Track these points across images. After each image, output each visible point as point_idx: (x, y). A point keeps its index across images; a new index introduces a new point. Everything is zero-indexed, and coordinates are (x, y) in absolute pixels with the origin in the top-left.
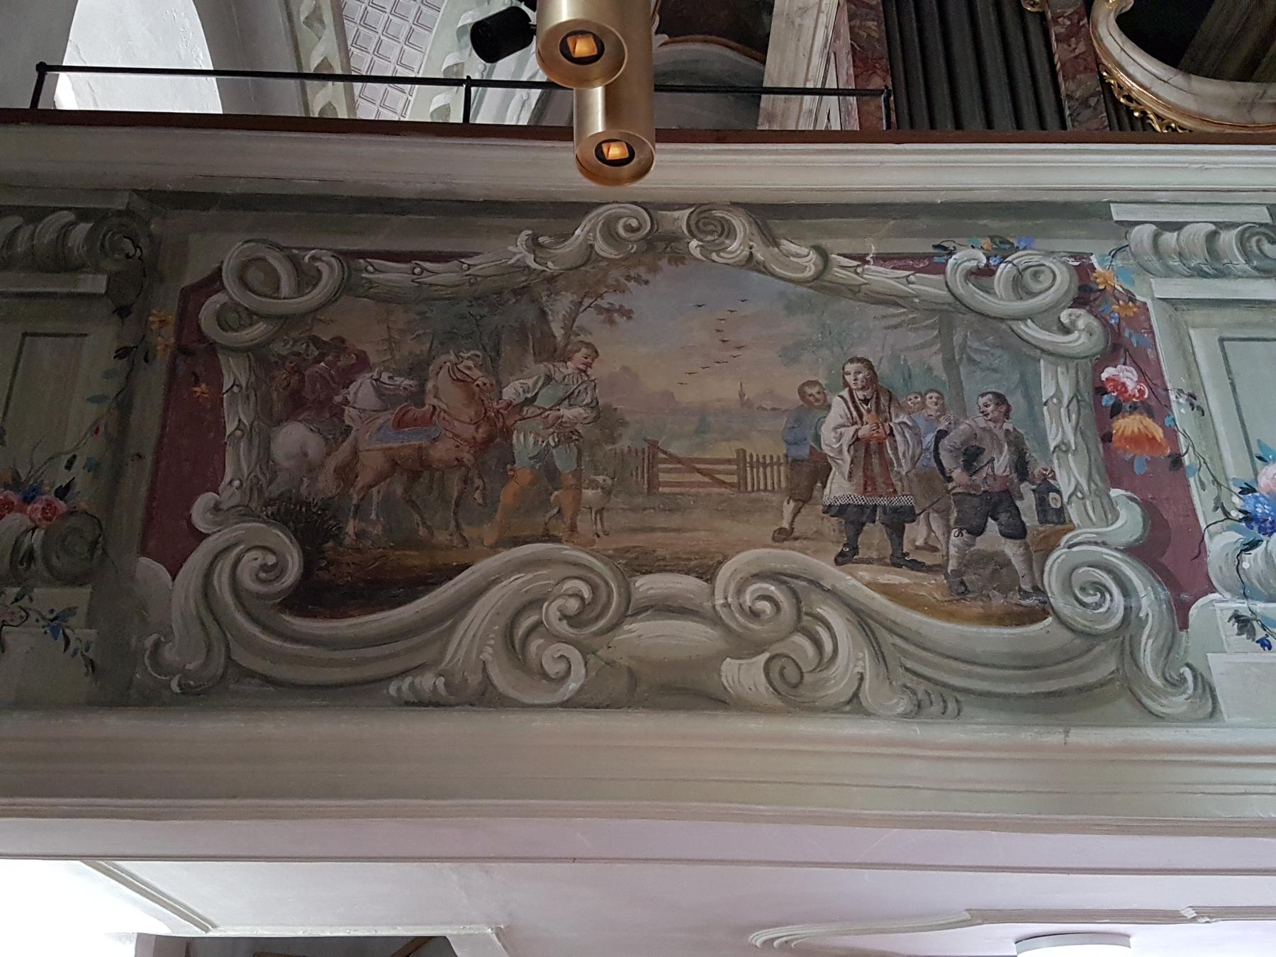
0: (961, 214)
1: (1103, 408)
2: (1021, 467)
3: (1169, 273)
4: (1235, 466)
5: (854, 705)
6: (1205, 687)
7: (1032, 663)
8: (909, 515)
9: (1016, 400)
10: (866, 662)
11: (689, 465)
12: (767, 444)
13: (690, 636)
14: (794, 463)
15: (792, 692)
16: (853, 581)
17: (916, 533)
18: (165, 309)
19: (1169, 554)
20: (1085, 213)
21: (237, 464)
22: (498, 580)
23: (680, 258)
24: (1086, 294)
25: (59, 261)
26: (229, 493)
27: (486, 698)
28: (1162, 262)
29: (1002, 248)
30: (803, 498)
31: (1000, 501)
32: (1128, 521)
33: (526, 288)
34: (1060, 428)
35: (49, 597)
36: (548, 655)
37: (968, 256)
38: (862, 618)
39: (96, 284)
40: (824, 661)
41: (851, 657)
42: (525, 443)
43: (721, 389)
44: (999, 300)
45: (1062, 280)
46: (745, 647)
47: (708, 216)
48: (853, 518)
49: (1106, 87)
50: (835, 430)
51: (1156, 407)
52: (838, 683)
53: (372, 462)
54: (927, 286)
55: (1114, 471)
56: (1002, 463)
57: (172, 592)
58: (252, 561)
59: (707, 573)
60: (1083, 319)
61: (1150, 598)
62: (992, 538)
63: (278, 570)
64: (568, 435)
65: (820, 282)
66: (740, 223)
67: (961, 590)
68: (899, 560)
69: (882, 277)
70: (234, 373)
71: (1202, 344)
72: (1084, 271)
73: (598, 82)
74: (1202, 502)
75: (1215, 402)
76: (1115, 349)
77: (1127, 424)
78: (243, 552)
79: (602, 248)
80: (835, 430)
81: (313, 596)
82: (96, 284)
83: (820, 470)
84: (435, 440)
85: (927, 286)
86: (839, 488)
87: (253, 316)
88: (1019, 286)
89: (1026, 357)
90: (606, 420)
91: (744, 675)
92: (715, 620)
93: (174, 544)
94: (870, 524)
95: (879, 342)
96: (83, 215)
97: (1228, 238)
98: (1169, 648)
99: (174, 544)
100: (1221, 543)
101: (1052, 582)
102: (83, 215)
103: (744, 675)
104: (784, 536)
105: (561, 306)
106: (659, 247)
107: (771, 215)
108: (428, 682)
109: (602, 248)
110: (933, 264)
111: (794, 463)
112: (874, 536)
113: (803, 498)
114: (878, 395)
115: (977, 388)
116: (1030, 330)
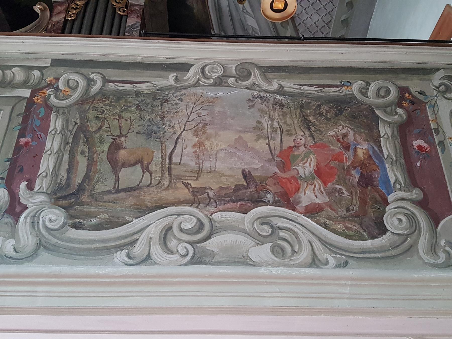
50: (371, 153)
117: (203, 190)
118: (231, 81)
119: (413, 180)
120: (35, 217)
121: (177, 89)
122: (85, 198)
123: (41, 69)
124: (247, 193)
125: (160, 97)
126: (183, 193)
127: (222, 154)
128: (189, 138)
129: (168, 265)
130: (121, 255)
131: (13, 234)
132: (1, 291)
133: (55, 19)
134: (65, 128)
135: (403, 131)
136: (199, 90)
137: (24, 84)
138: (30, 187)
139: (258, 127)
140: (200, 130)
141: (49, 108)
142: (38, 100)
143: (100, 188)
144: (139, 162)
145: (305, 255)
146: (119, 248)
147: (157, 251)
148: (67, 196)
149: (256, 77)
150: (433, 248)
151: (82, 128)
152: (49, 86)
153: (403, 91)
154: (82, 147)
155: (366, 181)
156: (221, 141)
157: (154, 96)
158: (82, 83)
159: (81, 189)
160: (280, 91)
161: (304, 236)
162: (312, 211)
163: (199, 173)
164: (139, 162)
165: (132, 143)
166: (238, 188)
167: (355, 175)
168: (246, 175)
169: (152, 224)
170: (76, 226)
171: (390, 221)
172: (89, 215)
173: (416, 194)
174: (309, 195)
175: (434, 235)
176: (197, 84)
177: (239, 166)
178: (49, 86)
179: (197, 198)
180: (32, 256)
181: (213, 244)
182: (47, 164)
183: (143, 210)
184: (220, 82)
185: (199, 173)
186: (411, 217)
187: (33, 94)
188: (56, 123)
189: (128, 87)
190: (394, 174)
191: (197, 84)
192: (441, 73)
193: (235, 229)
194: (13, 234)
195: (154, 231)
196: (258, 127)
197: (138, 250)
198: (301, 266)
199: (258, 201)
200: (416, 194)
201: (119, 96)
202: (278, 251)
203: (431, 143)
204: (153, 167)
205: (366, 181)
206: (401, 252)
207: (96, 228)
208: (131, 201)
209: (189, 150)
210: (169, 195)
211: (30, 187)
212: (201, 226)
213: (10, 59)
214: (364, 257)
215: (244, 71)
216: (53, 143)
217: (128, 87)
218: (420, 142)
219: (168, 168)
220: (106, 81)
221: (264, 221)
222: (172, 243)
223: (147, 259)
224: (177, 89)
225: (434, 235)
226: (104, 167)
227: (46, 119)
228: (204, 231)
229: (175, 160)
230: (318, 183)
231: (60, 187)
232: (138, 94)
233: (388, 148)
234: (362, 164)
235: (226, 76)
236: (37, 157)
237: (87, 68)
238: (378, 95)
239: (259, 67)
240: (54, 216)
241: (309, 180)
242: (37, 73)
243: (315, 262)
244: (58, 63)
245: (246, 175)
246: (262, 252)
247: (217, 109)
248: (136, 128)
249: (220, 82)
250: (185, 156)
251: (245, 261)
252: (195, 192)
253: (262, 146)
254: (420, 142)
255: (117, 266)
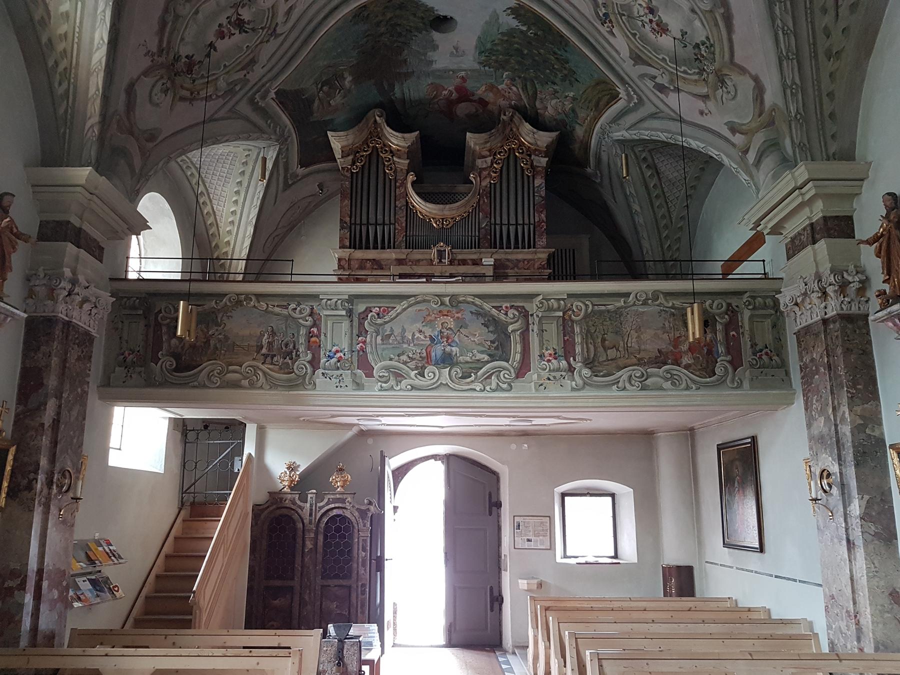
0: (293, 297)
1: (310, 335)
2: (294, 347)
3: (328, 309)
4: (329, 348)
5: (261, 387)
6: (315, 384)
7: (290, 380)
8: (275, 355)
9: (296, 335)
10: (264, 381)
11: (239, 346)
12: (253, 343)
13: (237, 376)
14: (257, 346)
15: (252, 386)
16: (263, 367)
17: (275, 359)
18: (152, 318)
19: (314, 363)
20: (315, 297)
21: (165, 346)
22: (207, 366)
23: (242, 305)
24: (311, 314)
25: (133, 308)
26: (164, 353)
27: (204, 386)
28: (327, 307)
29: (299, 304)
30: (258, 352)
31: (290, 354)
32: (309, 357)
33: (213, 312)
34: (302, 340)
35: (138, 369)
36: (214, 379)
37: (293, 306)
38: (264, 373)
39: (140, 312)
40: (258, 380)
41: (262, 379)
42: (212, 342)
43: (247, 332)
44: (297, 315)
45: (308, 311)
46: (245, 378)
47: (248, 297)
48: (266, 356)
49: (407, 203)
50: (265, 341)
51: (318, 336)
52: (260, 385)
53: (187, 345)
54: (285, 312)
55: (309, 348)
56: (291, 347)
57: (156, 368)
58: (169, 363)
59: (241, 366)
60: (310, 319)
61: (309, 370)
62: (288, 360)
63: (171, 365)
64: (220, 341)
65: (266, 311)
66: (253, 298)
67: (281, 369)
68: (272, 364)
69: (277, 310)
70: (164, 329)
71: (329, 324)
72: (312, 309)
73: (251, 131)
74: (322, 353)
75: (328, 336)
76: (315, 325)
77: (313, 339)
78: (167, 362)
79: (228, 304)
80: (265, 341)
81: (177, 370)
82: (140, 312)
83: (262, 347)
84: (447, 360)
85: (285, 312)
86: (264, 351)
87: (167, 318)
88: (301, 312)
89: (299, 326)
90: (226, 338)
91: (245, 383)
92: (241, 374)
93: (156, 360)
94: (268, 358)
95: (275, 323)
96: (137, 298)
97: (339, 302)
98: (310, 378)
99: (156, 360)
100: (323, 360)
101: (295, 367)
102: (137, 298)
103: (245, 383)
104: (254, 359)
105: (220, 315)
106: (239, 303)
107: (260, 296)
108: (196, 383)
109: (228, 304)
110: (528, 177)
111: (257, 346)
112: (269, 359)
113: (258, 352)
114: (273, 333)
115: (290, 332)
116: (301, 321)
117: (642, 359)
118: (650, 301)
119: (728, 352)
120: (580, 372)
121: (626, 308)
122: (596, 364)
123: (563, 299)
124: (660, 360)
125: (618, 312)
126: (635, 361)
127: (649, 342)
128: (634, 334)
129: (632, 391)
130: (615, 387)
131: (574, 380)
132: (299, 672)
133: (484, 184)
134: (581, 331)
135: (727, 327)
136: (635, 308)
137: (558, 309)
138: (575, 360)
139: (664, 327)
140: (638, 330)
141: (573, 321)
142: (567, 317)
143: (601, 359)
144: (614, 346)
145: (684, 385)
146: (614, 384)
147: (627, 385)
148: (589, 363)
149: (662, 300)
150: (733, 381)
151: (588, 331)
152: (569, 309)
153: (729, 305)
154: (590, 341)
155: (710, 352)
156: (647, 335)
157: (615, 312)
158: (583, 307)
159: (594, 360)
160: (673, 307)
161: (684, 377)
162: (687, 367)
163: (639, 351)
164: (614, 346)
165: (609, 337)
166: (656, 357)
167: (705, 349)
168: (659, 351)
169: (624, 374)
170: (596, 376)
171: (717, 371)
172: (600, 371)
173: (729, 358)
174: (686, 360)
175: (734, 376)
176: (634, 305)
177: (657, 347)
178: (569, 309)
179: (640, 363)
180: (583, 388)
181: (649, 382)
182: (578, 349)
183: (620, 368)
184: (645, 303)
185: (639, 351)
186: (726, 368)
187: (564, 314)
188: (577, 329)
189: (603, 308)
190: (721, 349)
191: (634, 305)
192: (747, 294)
193: (657, 375)
194: (574, 380)
195: (625, 377)
196: (664, 327)
197: (620, 385)
198: (682, 390)
199: (665, 364)
200: (729, 358)
201: (601, 313)
202: (673, 384)
203: (738, 333)
204: (620, 349)
205: (710, 352)
206: (721, 383)
207: (603, 376)
208: (614, 365)
209: (634, 340)
210: (629, 361)
211: (575, 360)
212: (643, 375)
213: (549, 295)
214: (706, 386)
215: (656, 295)
216: (578, 339)
217: (603, 308)
218: (734, 333)
219: (627, 349)
220: (593, 305)
221: (668, 372)
222: (633, 382)
223: (624, 389)
224: (626, 308)
225: (734, 376)
226: (601, 349)
227: (572, 327)
228: (645, 377)
229: (629, 345)
230: (690, 354)
231: (586, 360)
232: (608, 311)
233: (720, 336)
234: (708, 345)
235: (647, 299)
236: (574, 345)
237: (895, 527)
238: (717, 308)
239: (663, 293)
240: (586, 372)
241: (686, 353)
242: (562, 302)
243: (688, 388)
244: (570, 296)
245: (659, 351)
246: (668, 385)
247: (645, 318)
248: (610, 330)
249: (645, 303)
250: (633, 343)
251: (661, 389)
252: (639, 360)
253: (665, 336)
254: (734, 333)
255: (614, 391)
